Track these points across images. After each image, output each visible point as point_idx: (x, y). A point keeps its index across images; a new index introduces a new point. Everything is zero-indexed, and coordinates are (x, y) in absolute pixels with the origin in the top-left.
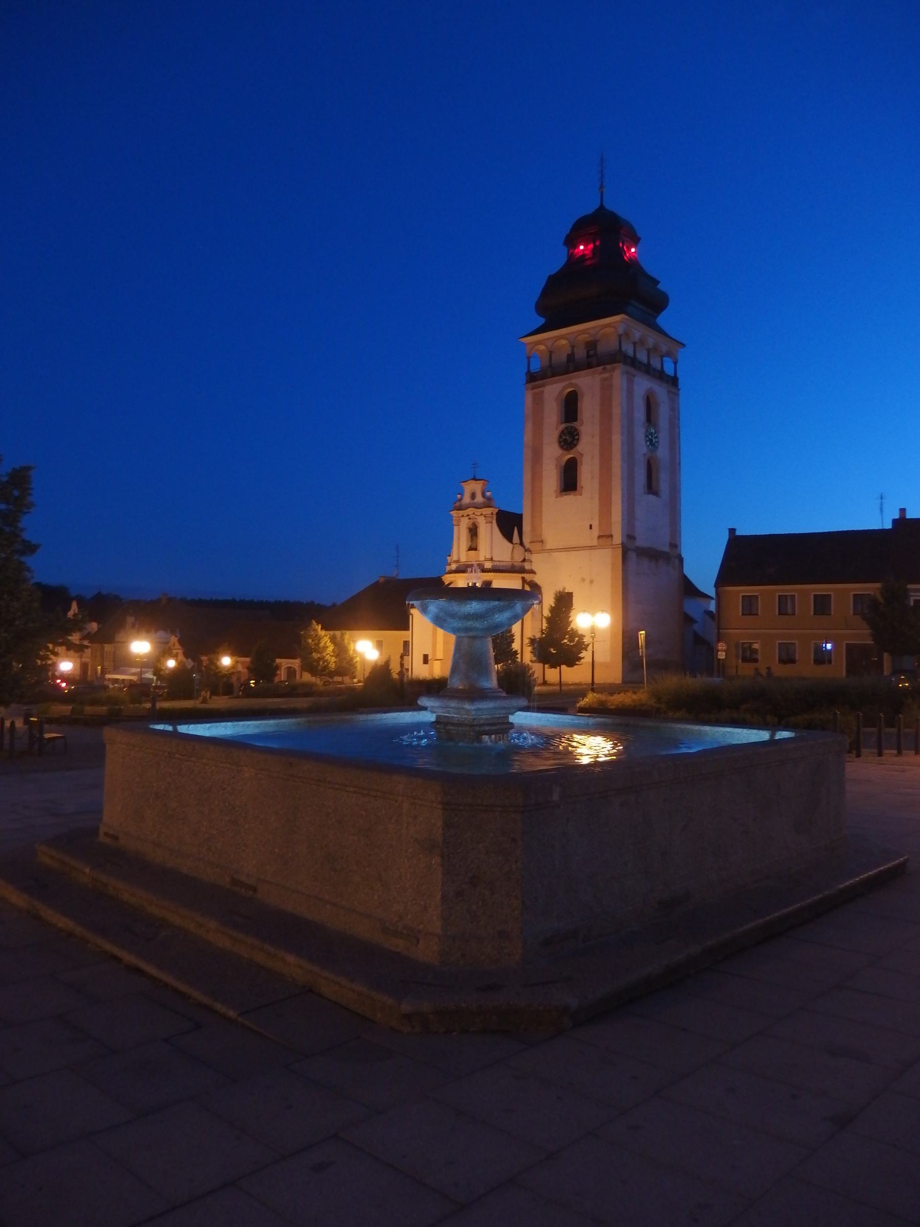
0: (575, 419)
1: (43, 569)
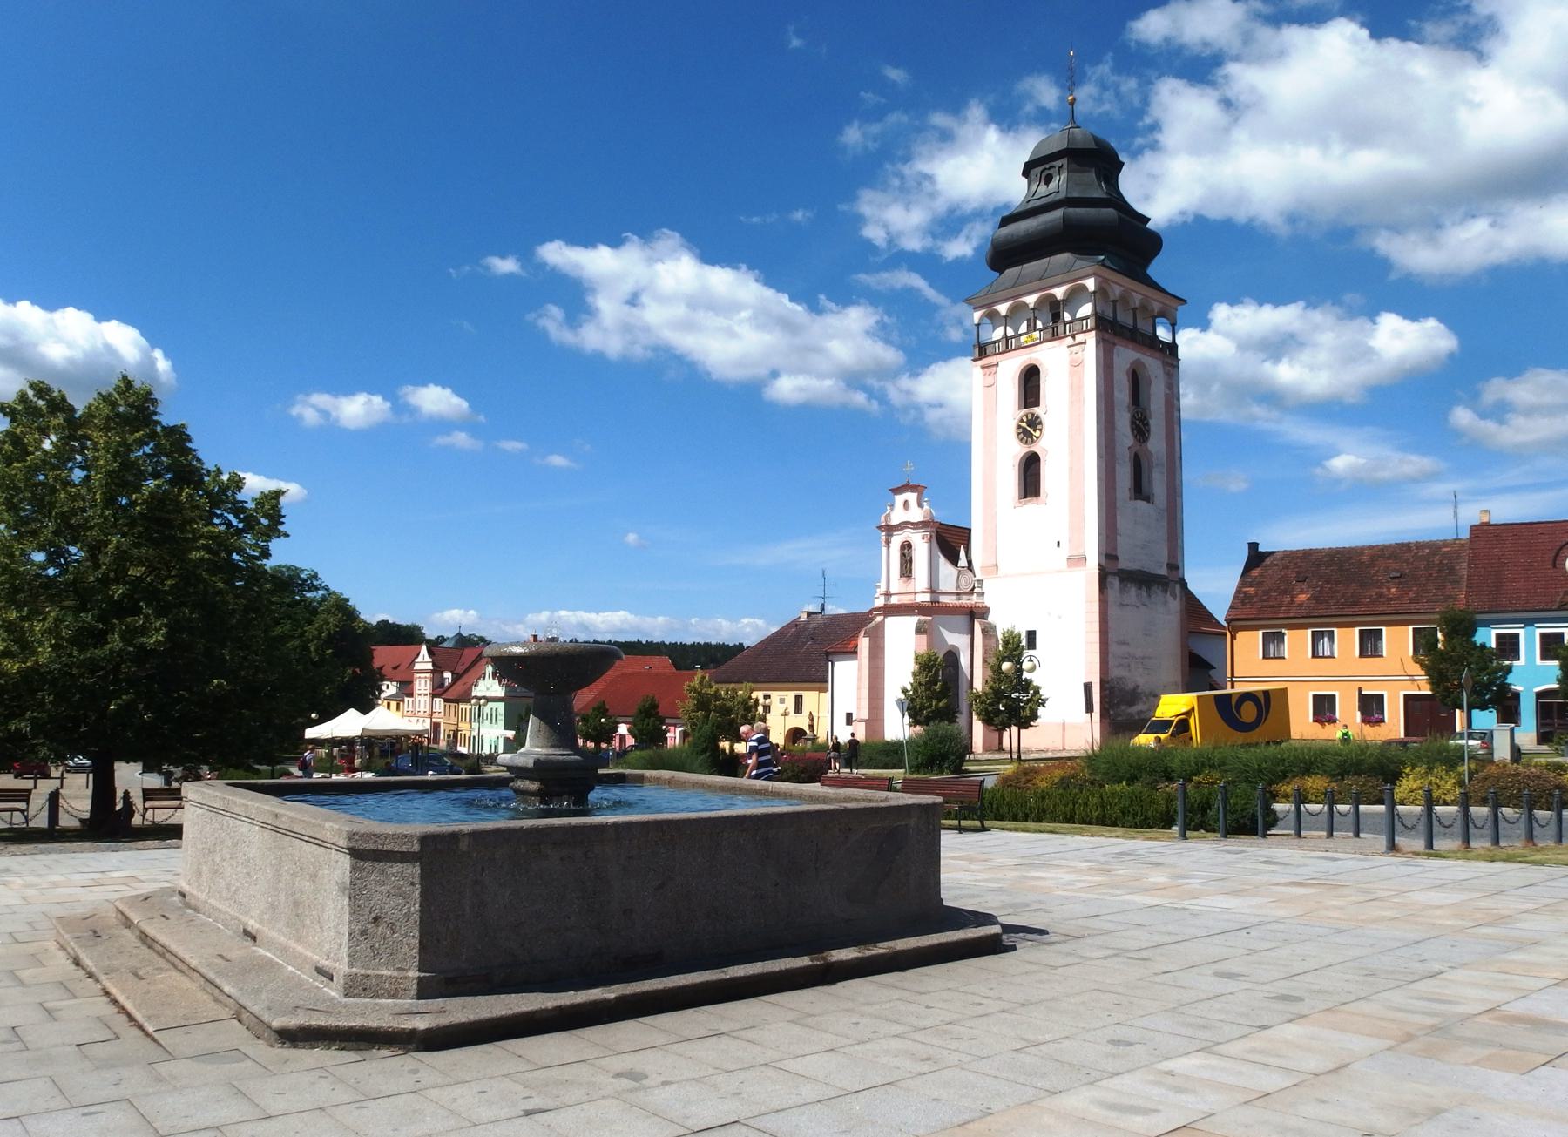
0: (1037, 404)
1: (415, 870)
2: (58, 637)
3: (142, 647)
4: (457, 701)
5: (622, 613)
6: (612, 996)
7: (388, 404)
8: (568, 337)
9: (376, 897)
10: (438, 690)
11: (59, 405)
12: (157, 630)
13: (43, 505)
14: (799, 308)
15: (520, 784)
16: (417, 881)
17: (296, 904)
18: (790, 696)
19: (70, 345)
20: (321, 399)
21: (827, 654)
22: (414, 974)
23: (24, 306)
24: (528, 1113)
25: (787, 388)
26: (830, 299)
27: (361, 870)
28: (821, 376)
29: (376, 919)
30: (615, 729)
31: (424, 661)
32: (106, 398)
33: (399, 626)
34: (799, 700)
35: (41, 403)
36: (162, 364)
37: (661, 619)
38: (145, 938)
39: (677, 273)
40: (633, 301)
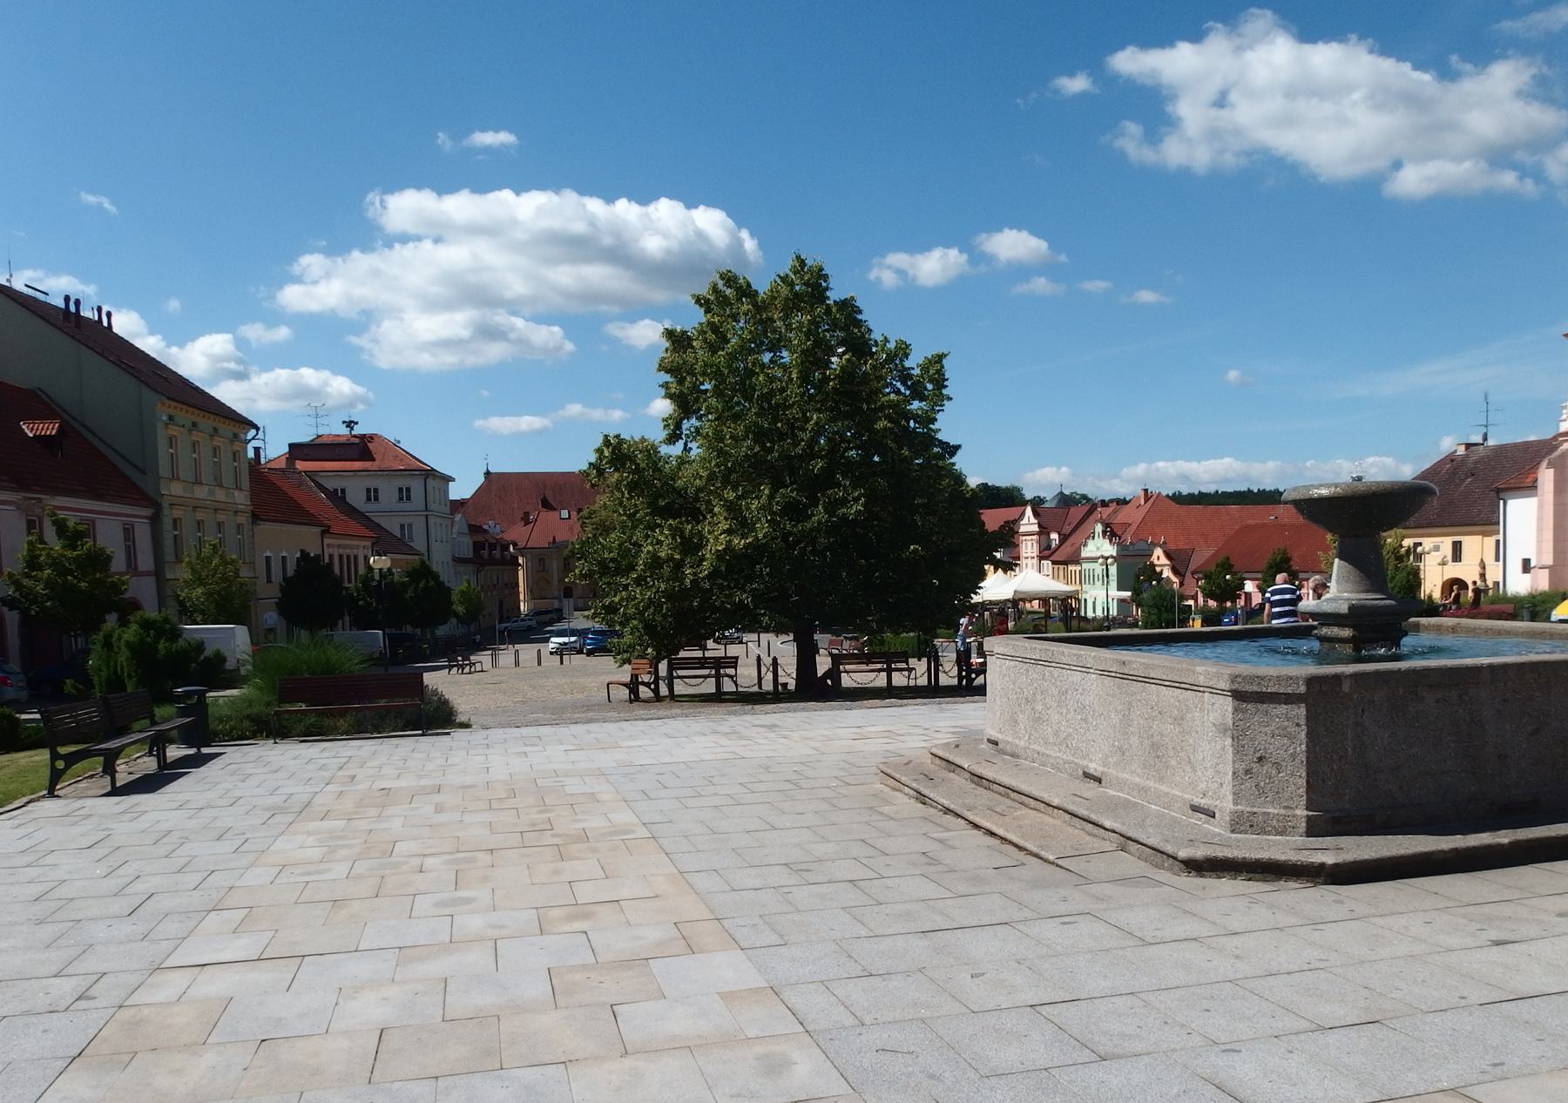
1: (1300, 711)
2: (773, 514)
3: (844, 517)
4: (1066, 563)
5: (1227, 460)
6: (1506, 841)
7: (965, 257)
8: (1148, 155)
9: (1261, 738)
10: (1045, 553)
11: (746, 291)
12: (856, 500)
13: (747, 392)
14: (1426, 77)
15: (1325, 631)
16: (1303, 721)
17: (1155, 746)
18: (1446, 543)
19: (666, 236)
20: (898, 259)
21: (1498, 491)
22: (1302, 812)
23: (622, 205)
24: (1498, 943)
25: (1412, 181)
26: (1464, 59)
27: (1245, 711)
28: (1458, 159)
29: (1260, 759)
30: (1242, 586)
31: (1029, 523)
32: (784, 279)
33: (998, 488)
34: (1457, 547)
35: (728, 291)
36: (750, 244)
37: (1271, 465)
38: (978, 778)
39: (1274, 57)
40: (1221, 101)
